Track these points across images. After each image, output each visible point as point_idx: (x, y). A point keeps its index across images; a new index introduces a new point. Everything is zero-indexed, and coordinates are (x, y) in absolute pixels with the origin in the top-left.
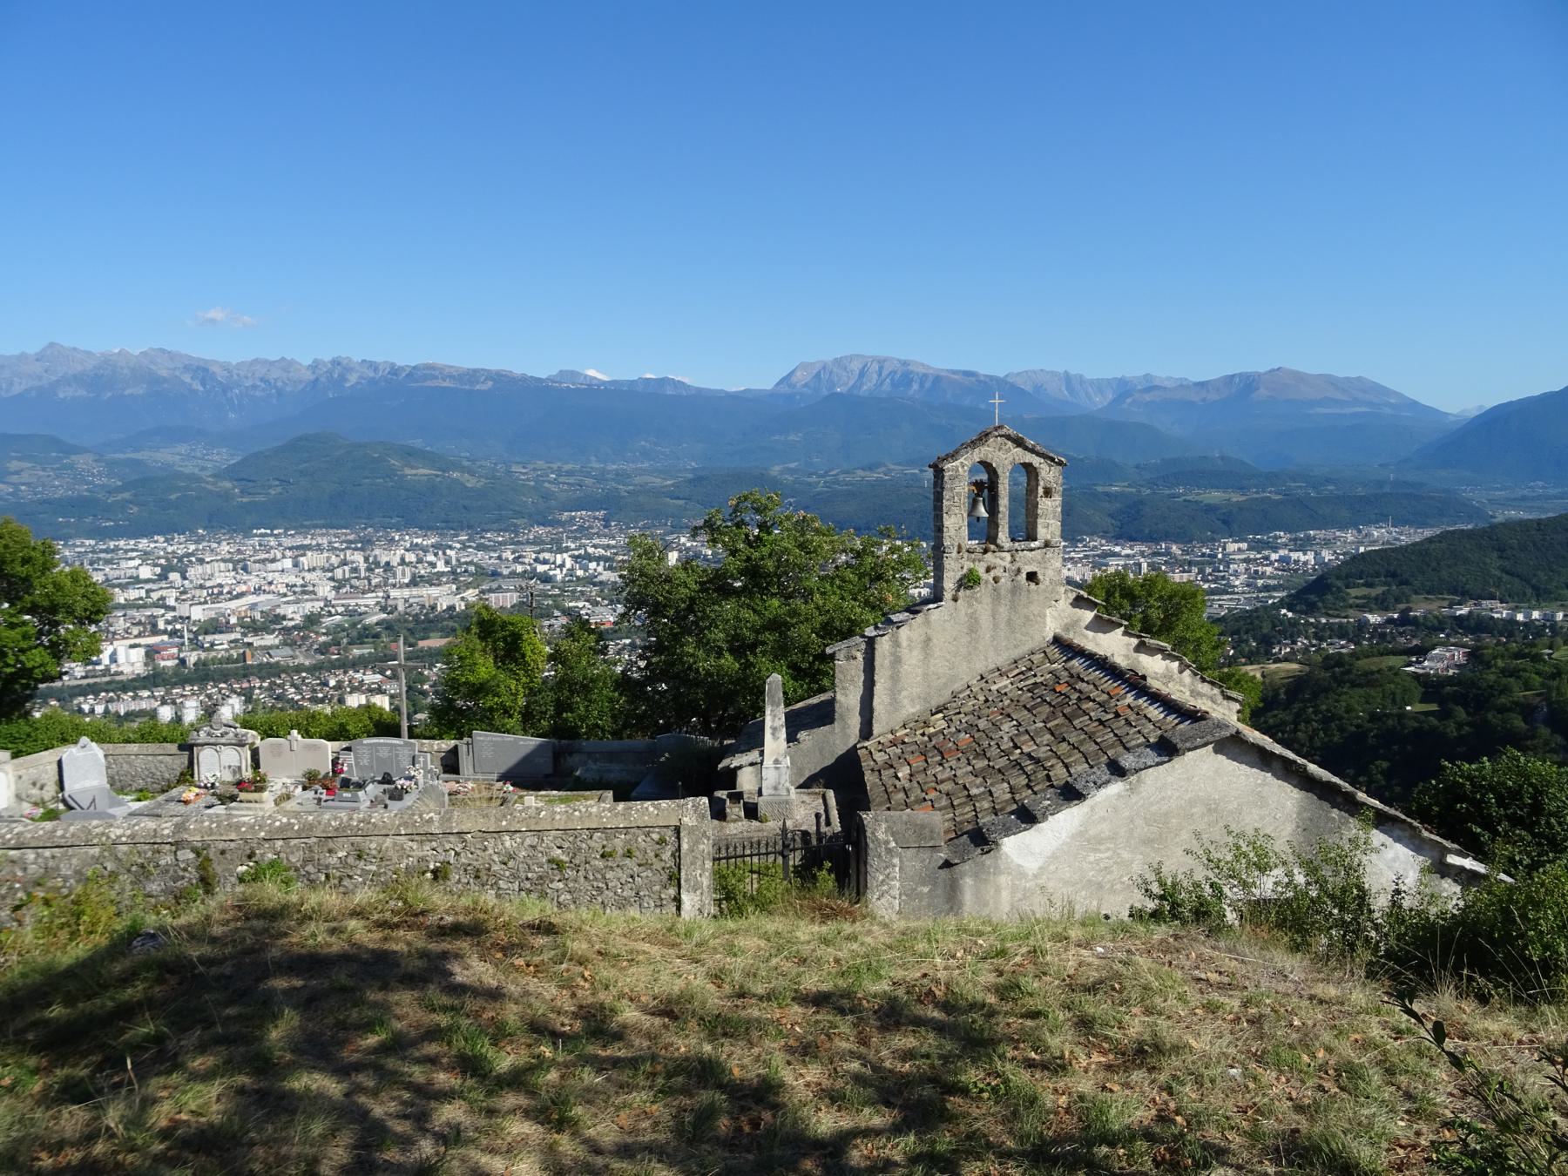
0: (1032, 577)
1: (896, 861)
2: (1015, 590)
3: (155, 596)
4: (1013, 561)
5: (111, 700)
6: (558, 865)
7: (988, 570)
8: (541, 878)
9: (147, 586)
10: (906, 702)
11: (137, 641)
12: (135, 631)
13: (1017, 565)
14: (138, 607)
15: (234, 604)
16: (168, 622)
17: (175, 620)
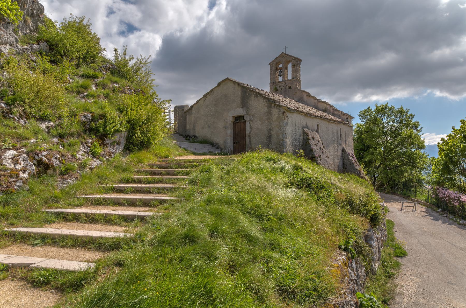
0: (290, 88)
7: (280, 87)
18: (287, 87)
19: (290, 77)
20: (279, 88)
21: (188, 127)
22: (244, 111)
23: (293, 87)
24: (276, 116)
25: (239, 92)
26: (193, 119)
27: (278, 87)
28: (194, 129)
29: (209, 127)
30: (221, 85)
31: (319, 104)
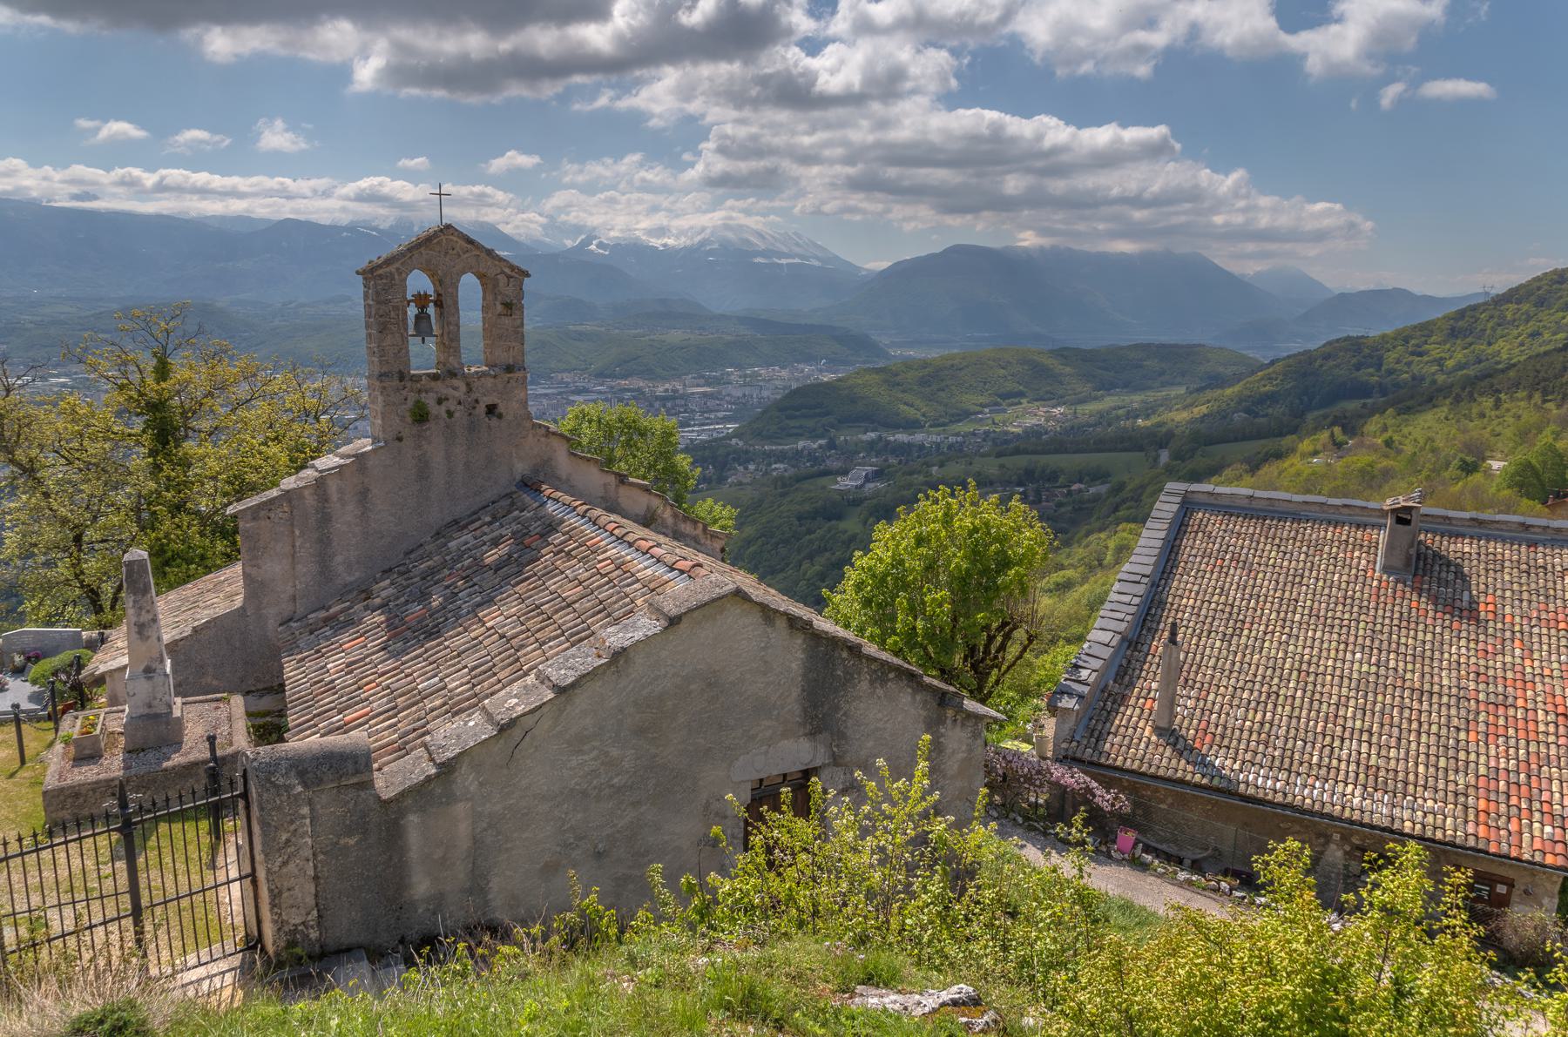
0: (491, 410)
7: (440, 402)
18: (481, 409)
19: (473, 352)
20: (434, 409)
24: (961, 756)
25: (792, 657)
26: (463, 829)
27: (429, 400)
29: (599, 855)
30: (683, 626)
31: (623, 490)
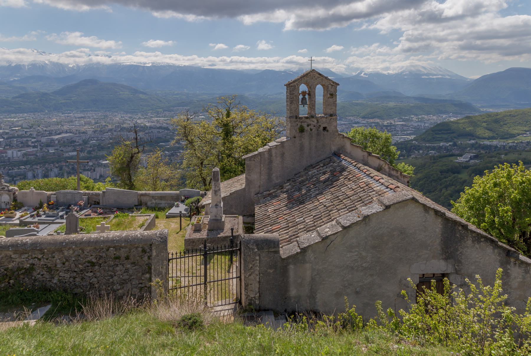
0: (325, 129)
1: (258, 258)
2: (318, 134)
3: (28, 133)
4: (318, 122)
5: (10, 170)
6: (93, 264)
7: (308, 126)
8: (81, 271)
9: (26, 130)
10: (274, 178)
11: (21, 149)
12: (20, 145)
13: (319, 124)
14: (22, 137)
15: (57, 137)
16: (32, 143)
17: (36, 142)
18: (321, 128)
21: (293, 292)
22: (450, 266)
23: (331, 128)
24: (519, 280)
26: (308, 273)
27: (305, 125)
28: (312, 296)
29: (357, 293)
31: (370, 158)
